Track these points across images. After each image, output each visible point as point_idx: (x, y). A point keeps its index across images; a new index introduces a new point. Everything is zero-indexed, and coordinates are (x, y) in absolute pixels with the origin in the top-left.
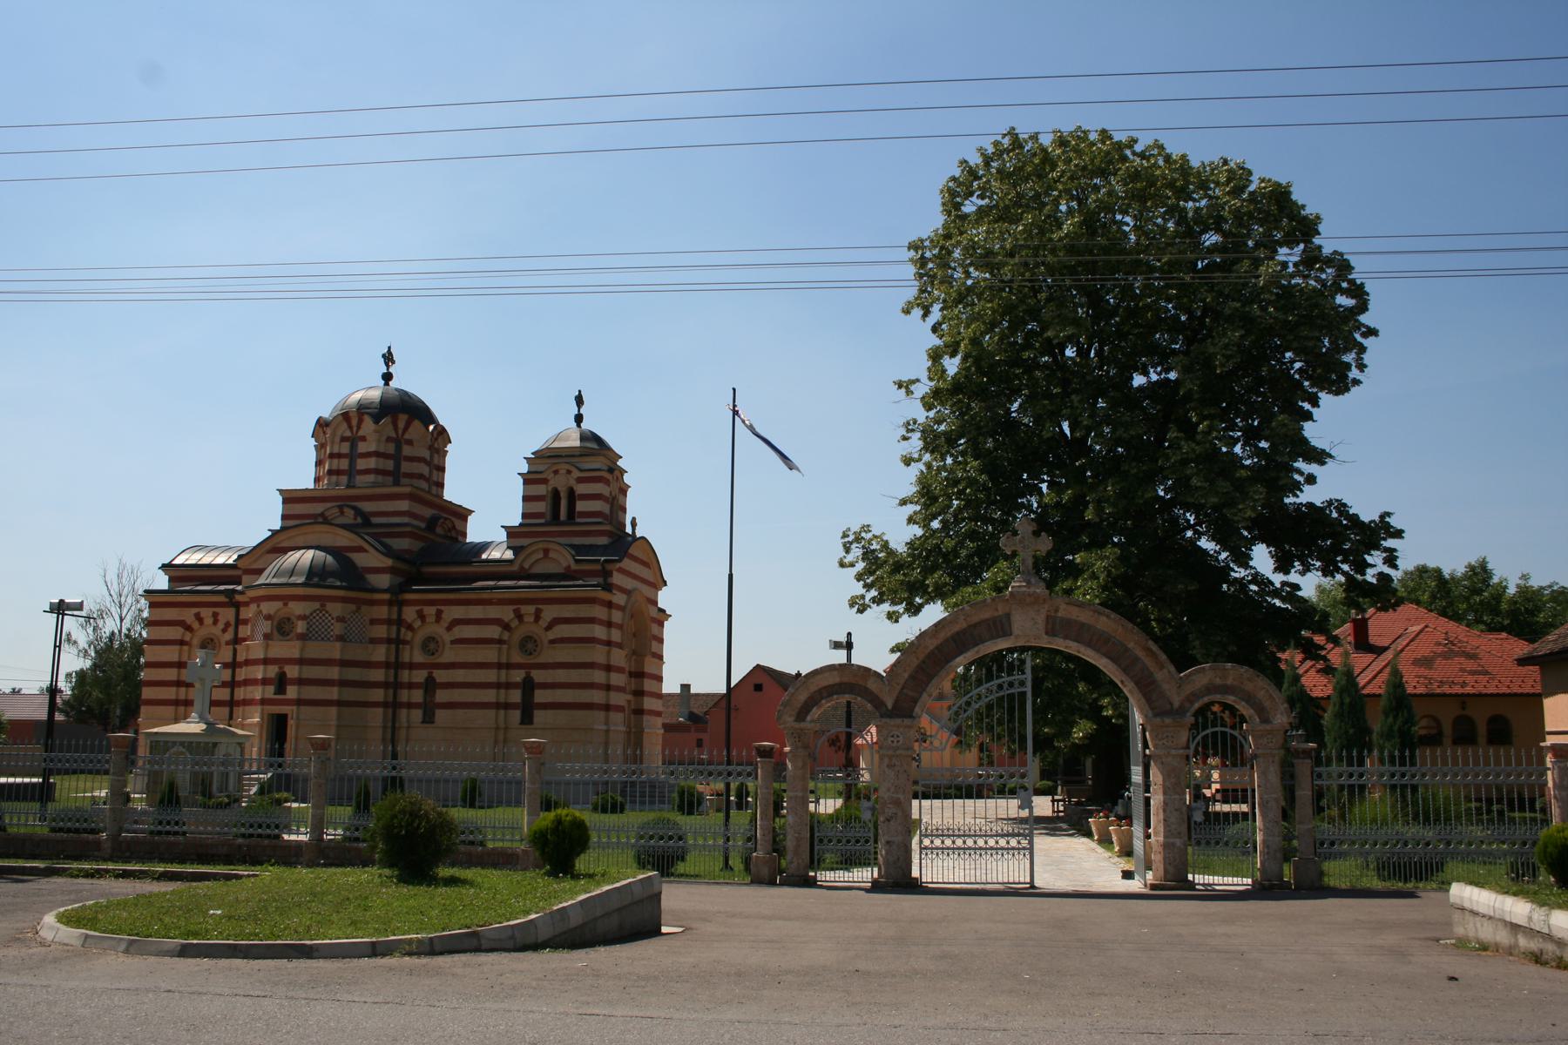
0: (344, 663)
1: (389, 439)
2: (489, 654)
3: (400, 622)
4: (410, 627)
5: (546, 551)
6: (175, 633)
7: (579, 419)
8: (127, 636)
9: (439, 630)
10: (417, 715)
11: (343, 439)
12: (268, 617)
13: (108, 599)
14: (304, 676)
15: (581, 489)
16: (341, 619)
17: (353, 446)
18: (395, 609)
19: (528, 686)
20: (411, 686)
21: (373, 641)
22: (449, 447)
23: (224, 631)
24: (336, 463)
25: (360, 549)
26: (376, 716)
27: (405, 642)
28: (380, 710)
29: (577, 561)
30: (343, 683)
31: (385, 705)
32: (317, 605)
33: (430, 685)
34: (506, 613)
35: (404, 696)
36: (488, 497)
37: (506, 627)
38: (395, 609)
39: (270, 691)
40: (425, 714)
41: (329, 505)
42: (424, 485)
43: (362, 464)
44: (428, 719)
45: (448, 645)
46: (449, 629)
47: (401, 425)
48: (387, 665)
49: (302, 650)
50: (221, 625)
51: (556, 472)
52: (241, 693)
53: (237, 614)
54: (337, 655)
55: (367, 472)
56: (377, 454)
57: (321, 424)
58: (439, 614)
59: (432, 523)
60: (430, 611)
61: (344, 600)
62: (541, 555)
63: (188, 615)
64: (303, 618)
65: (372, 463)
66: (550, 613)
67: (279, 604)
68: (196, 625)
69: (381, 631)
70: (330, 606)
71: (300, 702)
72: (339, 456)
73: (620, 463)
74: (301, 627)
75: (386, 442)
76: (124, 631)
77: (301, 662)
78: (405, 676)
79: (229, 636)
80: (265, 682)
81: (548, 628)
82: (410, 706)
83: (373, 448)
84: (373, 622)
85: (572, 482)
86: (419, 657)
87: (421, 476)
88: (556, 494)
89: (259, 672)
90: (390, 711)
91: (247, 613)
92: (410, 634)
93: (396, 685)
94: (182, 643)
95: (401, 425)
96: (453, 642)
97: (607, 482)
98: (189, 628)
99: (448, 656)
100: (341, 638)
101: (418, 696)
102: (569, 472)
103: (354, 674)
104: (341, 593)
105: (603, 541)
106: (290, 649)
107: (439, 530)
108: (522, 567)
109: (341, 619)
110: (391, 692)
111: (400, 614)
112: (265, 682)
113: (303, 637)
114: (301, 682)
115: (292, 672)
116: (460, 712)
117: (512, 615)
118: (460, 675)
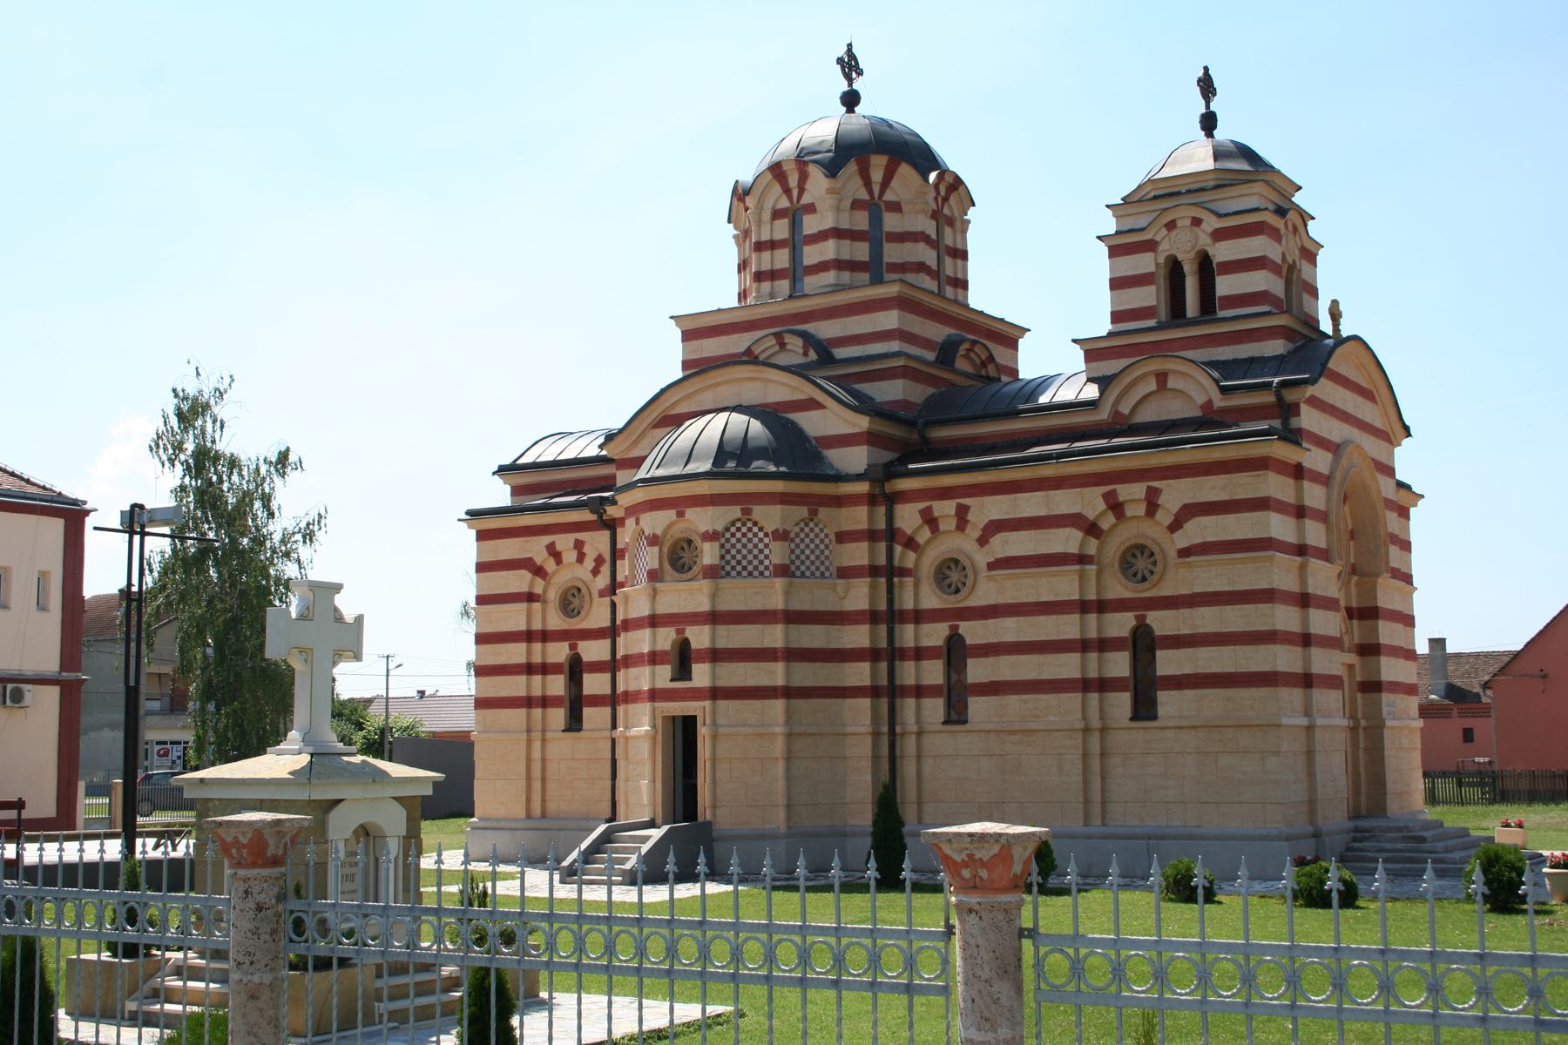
0: (792, 617)
1: (856, 205)
4: (910, 543)
5: (1162, 378)
6: (518, 581)
7: (1209, 122)
9: (964, 544)
10: (935, 708)
11: (777, 214)
12: (654, 540)
14: (722, 644)
15: (1223, 252)
16: (781, 536)
17: (795, 225)
20: (920, 654)
21: (845, 573)
22: (971, 214)
23: (595, 572)
25: (810, 405)
27: (904, 572)
28: (866, 702)
29: (1224, 390)
30: (792, 655)
31: (874, 692)
32: (736, 511)
33: (955, 652)
34: (1090, 502)
35: (908, 673)
36: (1046, 291)
37: (1092, 529)
39: (663, 676)
40: (949, 706)
41: (759, 334)
42: (929, 283)
44: (956, 715)
45: (984, 572)
46: (983, 541)
47: (877, 176)
48: (873, 617)
49: (714, 596)
50: (589, 563)
51: (1171, 226)
54: (778, 603)
55: (822, 267)
56: (837, 233)
58: (962, 513)
59: (947, 353)
60: (945, 509)
61: (784, 499)
62: (1152, 385)
63: (535, 549)
64: (711, 536)
67: (670, 515)
68: (550, 565)
69: (858, 554)
70: (758, 512)
71: (715, 693)
72: (773, 245)
73: (1298, 198)
74: (709, 554)
75: (863, 211)
77: (714, 618)
78: (908, 635)
79: (603, 581)
82: (920, 691)
84: (842, 537)
85: (1204, 241)
86: (931, 599)
87: (921, 267)
88: (1174, 269)
90: (884, 703)
92: (912, 556)
93: (893, 654)
94: (530, 597)
95: (877, 176)
96: (992, 566)
97: (1275, 235)
98: (539, 571)
99: (986, 592)
100: (783, 571)
101: (933, 672)
102: (1197, 222)
103: (813, 636)
104: (778, 486)
105: (1276, 347)
107: (961, 364)
108: (1116, 414)
109: (781, 536)
112: (654, 658)
113: (712, 573)
114: (716, 655)
115: (700, 637)
116: (1013, 701)
117: (1102, 506)
118: (1205, 620)
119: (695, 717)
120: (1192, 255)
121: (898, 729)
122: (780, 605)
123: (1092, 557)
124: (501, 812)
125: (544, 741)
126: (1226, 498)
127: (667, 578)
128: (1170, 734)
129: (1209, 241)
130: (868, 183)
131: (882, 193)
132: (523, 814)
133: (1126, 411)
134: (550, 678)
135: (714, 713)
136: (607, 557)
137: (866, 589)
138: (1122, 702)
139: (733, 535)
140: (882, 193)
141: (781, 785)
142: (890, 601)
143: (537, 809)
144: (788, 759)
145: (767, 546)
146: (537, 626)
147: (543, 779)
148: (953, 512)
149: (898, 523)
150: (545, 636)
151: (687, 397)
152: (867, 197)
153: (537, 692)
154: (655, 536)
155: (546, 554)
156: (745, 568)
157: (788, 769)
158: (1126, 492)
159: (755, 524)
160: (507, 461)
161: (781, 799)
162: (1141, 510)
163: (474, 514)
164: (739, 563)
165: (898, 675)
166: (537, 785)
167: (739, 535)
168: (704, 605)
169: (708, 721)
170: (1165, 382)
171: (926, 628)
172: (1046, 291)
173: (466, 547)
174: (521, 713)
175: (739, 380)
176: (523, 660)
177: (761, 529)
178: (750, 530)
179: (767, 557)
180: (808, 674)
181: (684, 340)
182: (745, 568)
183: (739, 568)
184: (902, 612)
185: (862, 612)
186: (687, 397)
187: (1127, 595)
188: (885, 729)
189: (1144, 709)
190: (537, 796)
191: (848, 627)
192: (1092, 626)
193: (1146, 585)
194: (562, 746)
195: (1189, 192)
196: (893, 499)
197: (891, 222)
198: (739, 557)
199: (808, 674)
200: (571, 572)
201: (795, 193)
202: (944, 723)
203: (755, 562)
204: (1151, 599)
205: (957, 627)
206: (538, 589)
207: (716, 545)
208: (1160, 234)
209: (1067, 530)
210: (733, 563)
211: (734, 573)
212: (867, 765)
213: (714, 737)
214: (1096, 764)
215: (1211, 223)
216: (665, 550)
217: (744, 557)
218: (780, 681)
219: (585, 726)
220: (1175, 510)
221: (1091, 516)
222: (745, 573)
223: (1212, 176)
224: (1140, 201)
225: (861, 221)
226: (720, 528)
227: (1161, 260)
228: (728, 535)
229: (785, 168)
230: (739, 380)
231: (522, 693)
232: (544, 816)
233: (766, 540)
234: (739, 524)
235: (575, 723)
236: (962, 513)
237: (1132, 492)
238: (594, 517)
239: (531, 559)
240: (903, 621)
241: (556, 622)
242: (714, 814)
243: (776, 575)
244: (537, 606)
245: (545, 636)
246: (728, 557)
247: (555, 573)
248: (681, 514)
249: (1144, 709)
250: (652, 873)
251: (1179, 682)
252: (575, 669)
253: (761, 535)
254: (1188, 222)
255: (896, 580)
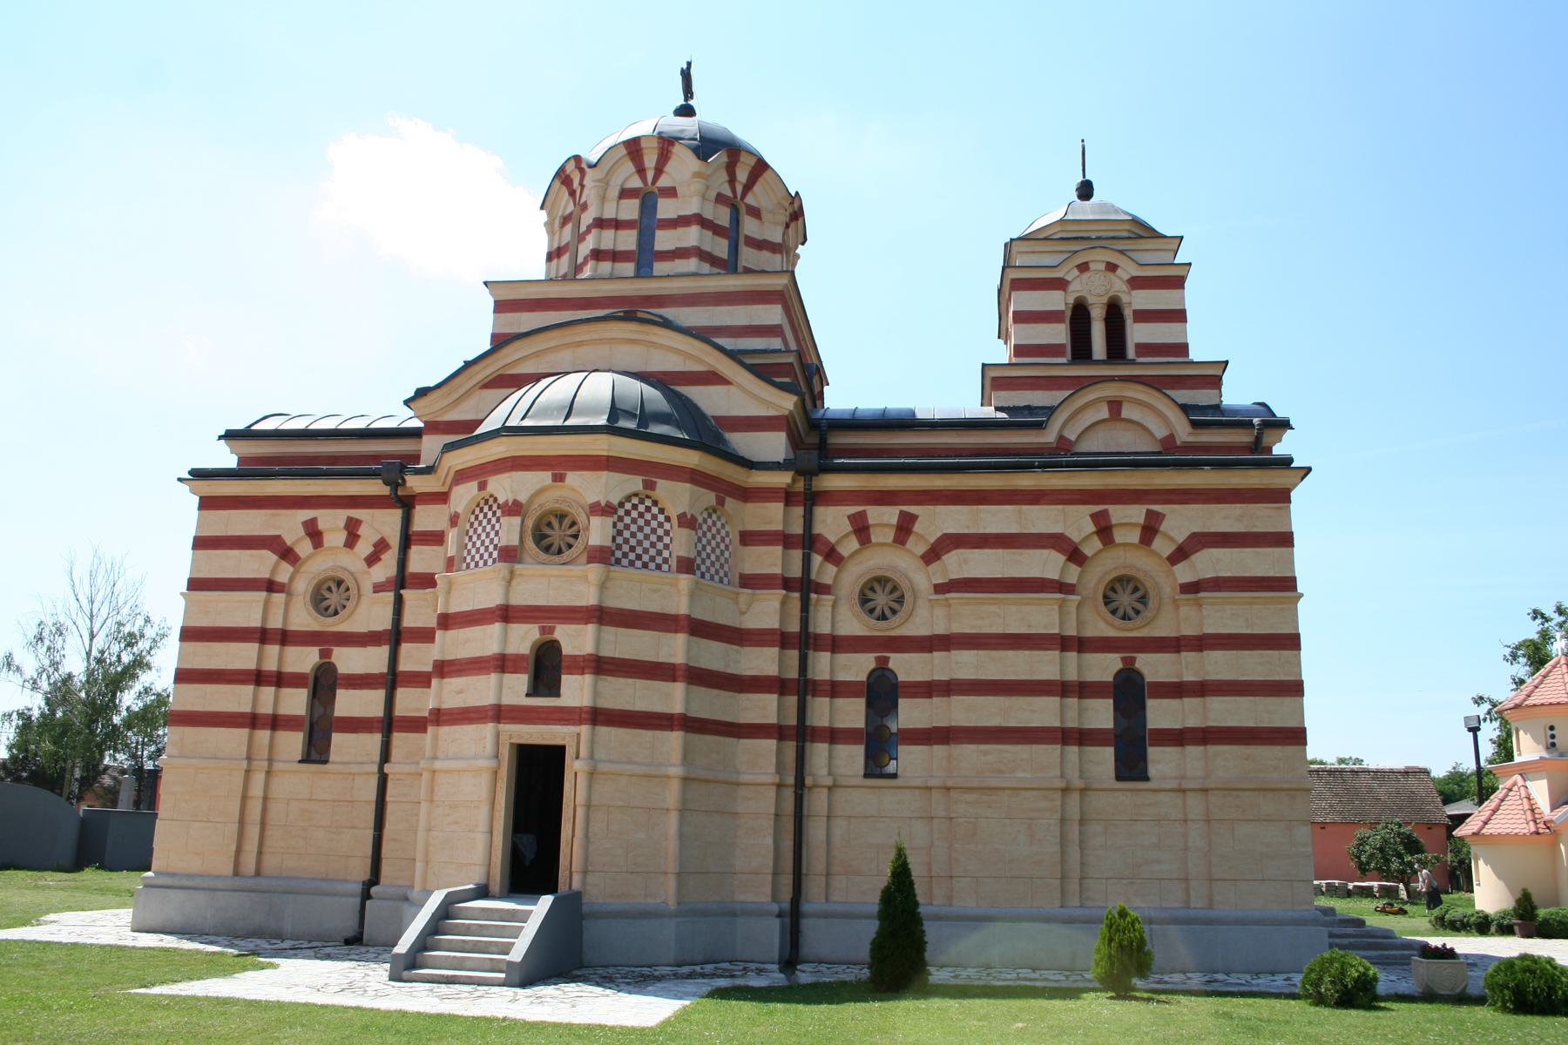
0: (699, 629)
1: (720, 199)
2: (1038, 615)
3: (809, 541)
4: (832, 555)
5: (1115, 406)
6: (258, 564)
8: (100, 661)
9: (904, 563)
10: (852, 757)
11: (625, 193)
12: (514, 509)
13: (74, 604)
14: (607, 652)
16: (687, 522)
18: (798, 511)
19: (1129, 692)
20: (836, 689)
21: (750, 582)
23: (372, 560)
24: (608, 239)
25: (712, 378)
26: (760, 761)
27: (824, 589)
28: (770, 744)
30: (697, 677)
31: (777, 732)
32: (635, 483)
33: (882, 692)
34: (1077, 523)
35: (822, 712)
36: (907, 329)
38: (798, 511)
39: (515, 690)
43: (665, 240)
44: (876, 766)
48: (782, 640)
49: (603, 586)
50: (364, 548)
51: (1083, 268)
52: (409, 702)
53: (407, 521)
54: (680, 605)
55: (680, 253)
56: (699, 220)
57: (569, 177)
60: (884, 517)
61: (696, 477)
62: (1104, 413)
63: (288, 526)
64: (606, 510)
65: (691, 236)
66: (1180, 522)
67: (545, 477)
68: (304, 548)
69: (769, 560)
70: (664, 488)
71: (597, 716)
72: (617, 224)
75: (682, 231)
76: (95, 653)
77: (601, 615)
78: (823, 665)
79: (386, 568)
80: (503, 664)
81: (1181, 554)
82: (834, 736)
83: (691, 207)
84: (748, 538)
86: (852, 623)
88: (1080, 313)
89: (487, 640)
90: (790, 747)
91: (425, 518)
92: (831, 569)
93: (803, 688)
94: (271, 586)
96: (940, 589)
98: (287, 554)
99: (923, 620)
101: (852, 713)
103: (714, 656)
106: (576, 584)
108: (1061, 438)
109: (687, 522)
110: (792, 701)
111: (808, 520)
112: (503, 664)
113: (601, 555)
114: (600, 666)
115: (576, 640)
116: (969, 753)
118: (1189, 667)
119: (562, 749)
120: (1105, 300)
121: (808, 781)
122: (683, 609)
123: (1073, 586)
124: (193, 865)
125: (269, 773)
126: (1243, 530)
127: (527, 558)
128: (1163, 797)
129: (1124, 288)
130: (732, 181)
131: (654, 182)
132: (229, 870)
133: (1073, 438)
134: (286, 692)
135: (592, 742)
136: (395, 541)
137: (777, 604)
138: (1105, 757)
139: (628, 513)
140: (744, 195)
141: (672, 845)
142: (805, 621)
143: (249, 865)
144: (684, 810)
145: (667, 533)
146: (275, 623)
147: (263, 824)
148: (894, 521)
149: (818, 529)
150: (285, 638)
151: (537, 354)
152: (729, 194)
153: (266, 708)
154: (516, 503)
155: (302, 532)
156: (639, 557)
157: (682, 823)
158: (1118, 513)
159: (655, 503)
160: (240, 425)
161: (672, 866)
162: (1134, 537)
163: (198, 474)
164: (632, 549)
165: (809, 713)
166: (253, 832)
167: (634, 514)
168: (589, 598)
169: (583, 752)
170: (1119, 413)
171: (843, 658)
172: (907, 329)
173: (183, 514)
174: (242, 734)
175: (612, 341)
176: (252, 666)
177: (662, 511)
178: (648, 509)
179: (666, 547)
180: (713, 704)
181: (496, 311)
182: (639, 557)
183: (632, 556)
184: (817, 636)
185: (771, 632)
186: (537, 354)
187: (1111, 633)
188: (791, 780)
189: (1131, 767)
190: (251, 847)
191: (747, 649)
192: (1070, 666)
193: (1138, 621)
194: (296, 782)
195: (1099, 238)
196: (812, 499)
197: (750, 227)
198: (633, 542)
199: (713, 704)
200: (335, 558)
201: (650, 175)
202: (866, 776)
203: (652, 552)
204: (1142, 639)
205: (887, 660)
206: (283, 576)
207: (609, 521)
208: (1071, 274)
209: (1045, 552)
210: (626, 548)
211: (625, 562)
212: (768, 824)
213: (592, 775)
214: (1074, 832)
215: (1128, 270)
216: (530, 523)
217: (640, 543)
218: (677, 708)
219: (333, 757)
220: (1180, 539)
221: (1075, 537)
222: (639, 564)
223: (1127, 227)
224: (1045, 239)
225: (723, 217)
226: (615, 502)
227: (1071, 301)
228: (621, 512)
229: (643, 144)
230: (612, 341)
231: (246, 708)
232: (258, 873)
233: (667, 526)
234: (635, 501)
235: (316, 751)
236: (352, 528)
237: (1128, 516)
238: (385, 490)
239: (278, 538)
240: (817, 648)
241: (303, 619)
242: (584, 883)
243: (679, 571)
244: (279, 598)
245: (285, 638)
246: (620, 540)
247: (310, 557)
248: (559, 478)
249: (1131, 767)
250: (533, 973)
251: (1178, 738)
252: (324, 683)
253: (661, 518)
254: (1102, 267)
255: (813, 596)
